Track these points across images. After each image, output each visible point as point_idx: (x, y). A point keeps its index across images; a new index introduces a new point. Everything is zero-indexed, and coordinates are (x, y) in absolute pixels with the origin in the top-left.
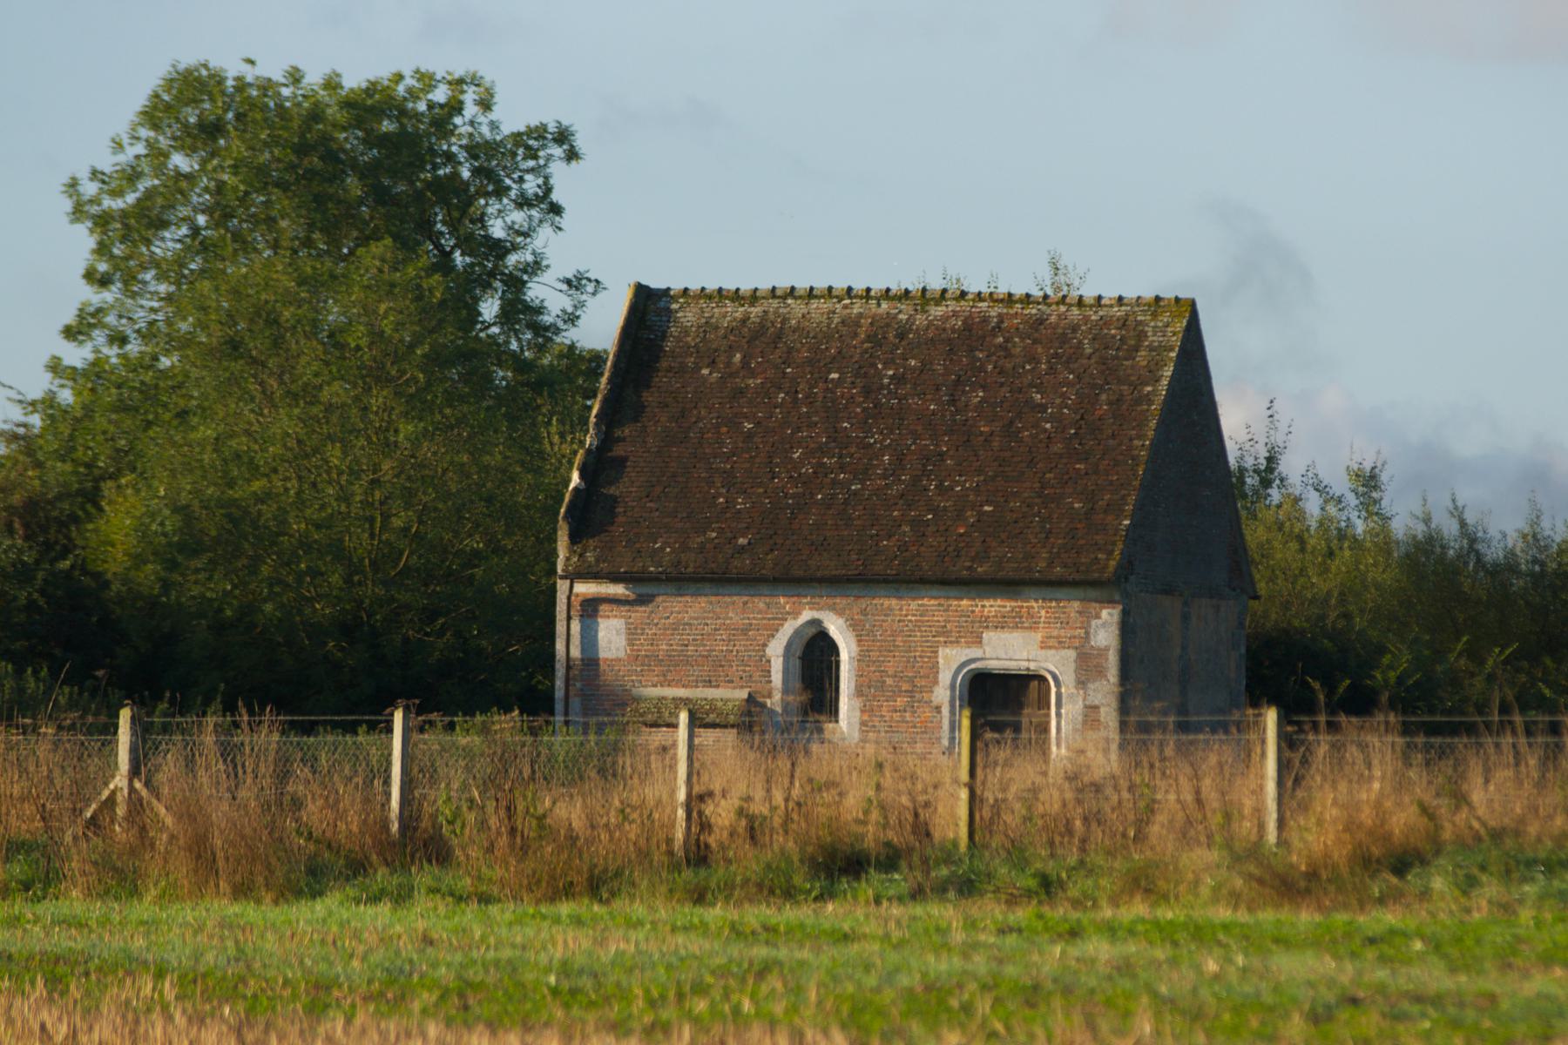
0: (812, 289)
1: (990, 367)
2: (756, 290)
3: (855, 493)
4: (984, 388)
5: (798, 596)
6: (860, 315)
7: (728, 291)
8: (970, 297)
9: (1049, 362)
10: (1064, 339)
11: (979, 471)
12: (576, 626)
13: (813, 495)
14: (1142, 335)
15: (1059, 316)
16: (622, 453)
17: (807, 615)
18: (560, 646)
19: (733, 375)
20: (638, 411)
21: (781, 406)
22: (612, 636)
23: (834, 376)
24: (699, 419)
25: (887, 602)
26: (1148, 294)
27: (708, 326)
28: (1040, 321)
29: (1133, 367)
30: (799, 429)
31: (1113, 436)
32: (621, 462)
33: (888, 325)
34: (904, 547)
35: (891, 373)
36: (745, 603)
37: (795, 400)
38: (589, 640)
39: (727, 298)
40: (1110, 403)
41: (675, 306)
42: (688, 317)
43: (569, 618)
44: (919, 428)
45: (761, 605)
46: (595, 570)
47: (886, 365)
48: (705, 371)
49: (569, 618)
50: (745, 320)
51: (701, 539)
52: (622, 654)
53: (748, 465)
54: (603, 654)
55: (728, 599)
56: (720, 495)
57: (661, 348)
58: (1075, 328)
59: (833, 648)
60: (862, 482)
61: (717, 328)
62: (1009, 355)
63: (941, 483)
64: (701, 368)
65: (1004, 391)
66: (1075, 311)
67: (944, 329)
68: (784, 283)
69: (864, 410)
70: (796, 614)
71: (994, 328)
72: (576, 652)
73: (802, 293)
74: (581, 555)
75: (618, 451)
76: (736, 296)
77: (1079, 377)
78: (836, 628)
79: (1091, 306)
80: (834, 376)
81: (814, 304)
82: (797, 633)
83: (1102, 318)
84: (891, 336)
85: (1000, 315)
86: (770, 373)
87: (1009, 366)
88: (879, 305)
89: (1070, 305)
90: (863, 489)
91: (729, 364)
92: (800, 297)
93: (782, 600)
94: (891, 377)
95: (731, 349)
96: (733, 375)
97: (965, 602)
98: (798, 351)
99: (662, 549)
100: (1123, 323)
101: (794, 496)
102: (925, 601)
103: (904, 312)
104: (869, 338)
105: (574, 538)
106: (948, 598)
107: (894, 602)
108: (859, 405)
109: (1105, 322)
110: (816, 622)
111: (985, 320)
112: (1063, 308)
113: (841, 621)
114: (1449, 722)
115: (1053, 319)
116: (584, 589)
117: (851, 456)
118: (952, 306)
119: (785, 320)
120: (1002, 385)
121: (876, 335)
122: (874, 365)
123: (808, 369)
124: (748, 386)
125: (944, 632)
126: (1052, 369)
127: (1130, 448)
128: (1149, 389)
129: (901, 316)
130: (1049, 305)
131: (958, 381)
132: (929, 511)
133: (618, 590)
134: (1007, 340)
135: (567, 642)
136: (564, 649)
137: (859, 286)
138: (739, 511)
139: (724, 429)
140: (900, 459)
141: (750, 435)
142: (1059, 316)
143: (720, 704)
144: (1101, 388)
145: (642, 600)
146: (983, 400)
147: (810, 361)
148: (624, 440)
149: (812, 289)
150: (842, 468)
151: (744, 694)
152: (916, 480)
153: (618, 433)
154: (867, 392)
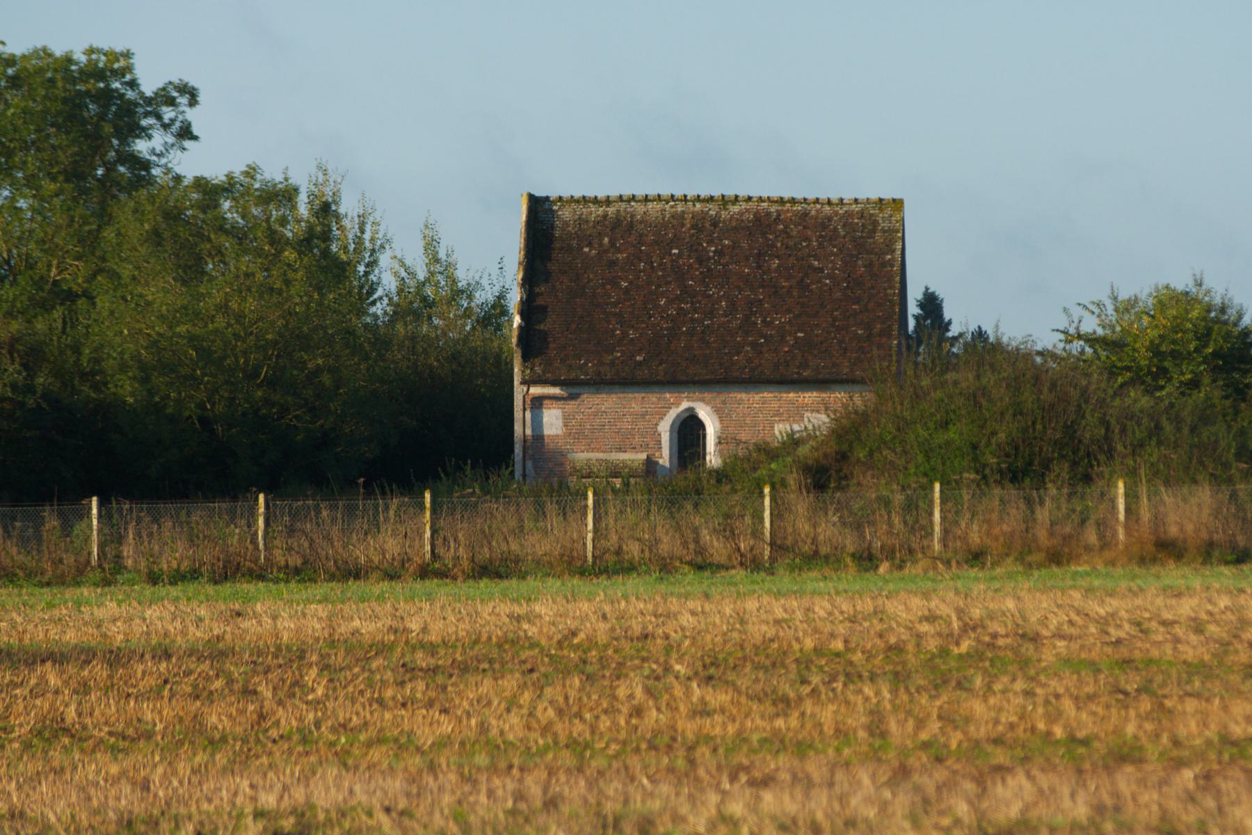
0: (647, 196)
1: (779, 245)
2: (608, 197)
3: (708, 326)
4: (778, 257)
5: (680, 392)
6: (683, 212)
7: (729, 196)
8: (755, 199)
9: (817, 241)
10: (824, 226)
11: (789, 311)
12: (528, 415)
13: (680, 328)
14: (875, 223)
15: (817, 211)
16: (543, 303)
17: (685, 405)
18: (518, 428)
19: (606, 251)
20: (547, 276)
21: (644, 271)
22: (553, 421)
23: (675, 251)
24: (590, 280)
25: (739, 396)
26: (874, 196)
27: (581, 221)
28: (805, 214)
29: (874, 243)
30: (659, 286)
31: (873, 288)
32: (544, 309)
33: (704, 218)
34: (750, 360)
35: (713, 249)
36: (643, 398)
37: (652, 267)
38: (537, 423)
39: (589, 202)
40: (865, 266)
41: (555, 208)
42: (566, 214)
43: (524, 410)
44: (741, 284)
45: (654, 399)
46: (543, 378)
47: (710, 243)
48: (586, 250)
49: (524, 410)
50: (605, 216)
51: (610, 357)
52: (560, 432)
53: (630, 310)
54: (547, 431)
55: (630, 395)
56: (616, 329)
57: (553, 235)
58: (830, 219)
59: (701, 425)
60: (711, 319)
61: (587, 222)
62: (789, 237)
63: (765, 318)
64: (582, 248)
65: (792, 260)
66: (827, 208)
67: (742, 221)
68: (627, 192)
69: (701, 273)
70: (678, 404)
71: (775, 220)
72: (529, 432)
73: (640, 198)
74: (532, 369)
75: (540, 301)
76: (596, 201)
77: (840, 250)
78: (705, 414)
79: (837, 205)
80: (675, 251)
81: (650, 205)
82: (678, 416)
83: (846, 212)
84: (707, 225)
85: (777, 211)
86: (631, 250)
87: (791, 243)
88: (694, 205)
89: (823, 204)
90: (712, 324)
91: (601, 245)
92: (639, 201)
93: (668, 395)
94: (714, 252)
95: (601, 235)
96: (606, 251)
97: (791, 395)
98: (647, 236)
99: (586, 364)
100: (861, 215)
101: (667, 329)
102: (765, 394)
103: (713, 210)
104: (693, 227)
105: (525, 358)
106: (780, 392)
107: (744, 396)
108: (697, 270)
109: (849, 214)
110: (691, 410)
111: (768, 214)
112: (818, 206)
113: (708, 408)
114: (932, 502)
115: (813, 213)
116: (536, 390)
117: (700, 302)
118: (744, 205)
119: (632, 216)
120: (790, 255)
121: (697, 225)
122: (702, 245)
123: (656, 247)
124: (618, 259)
125: (777, 414)
126: (820, 245)
127: (886, 295)
128: (889, 257)
129: (711, 212)
130: (809, 204)
131: (759, 255)
132: (762, 337)
133: (555, 391)
134: (786, 227)
135: (521, 427)
136: (522, 430)
137: (679, 193)
138: (632, 339)
139: (609, 287)
140: (733, 305)
141: (627, 290)
142: (817, 211)
143: (629, 463)
144: (857, 256)
145: (572, 397)
146: (779, 266)
147: (656, 242)
148: (542, 294)
149: (647, 196)
150: (695, 311)
151: (643, 456)
152: (747, 318)
153: (537, 290)
154: (700, 261)
